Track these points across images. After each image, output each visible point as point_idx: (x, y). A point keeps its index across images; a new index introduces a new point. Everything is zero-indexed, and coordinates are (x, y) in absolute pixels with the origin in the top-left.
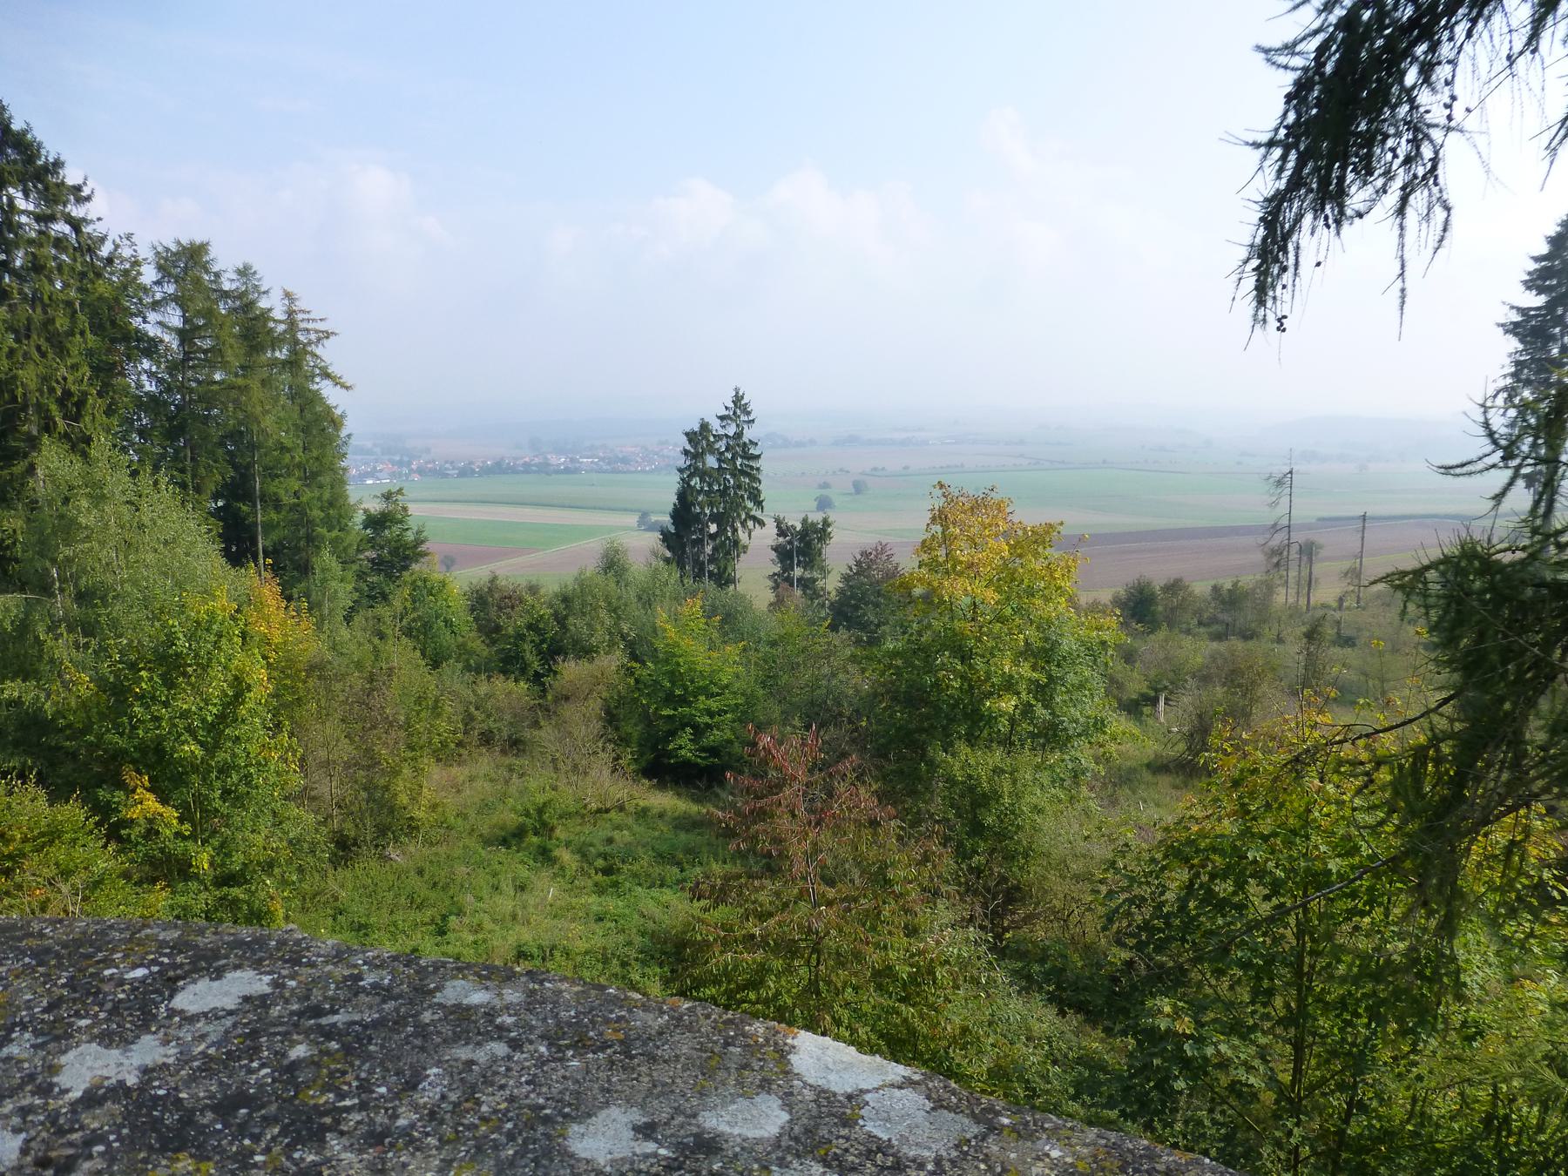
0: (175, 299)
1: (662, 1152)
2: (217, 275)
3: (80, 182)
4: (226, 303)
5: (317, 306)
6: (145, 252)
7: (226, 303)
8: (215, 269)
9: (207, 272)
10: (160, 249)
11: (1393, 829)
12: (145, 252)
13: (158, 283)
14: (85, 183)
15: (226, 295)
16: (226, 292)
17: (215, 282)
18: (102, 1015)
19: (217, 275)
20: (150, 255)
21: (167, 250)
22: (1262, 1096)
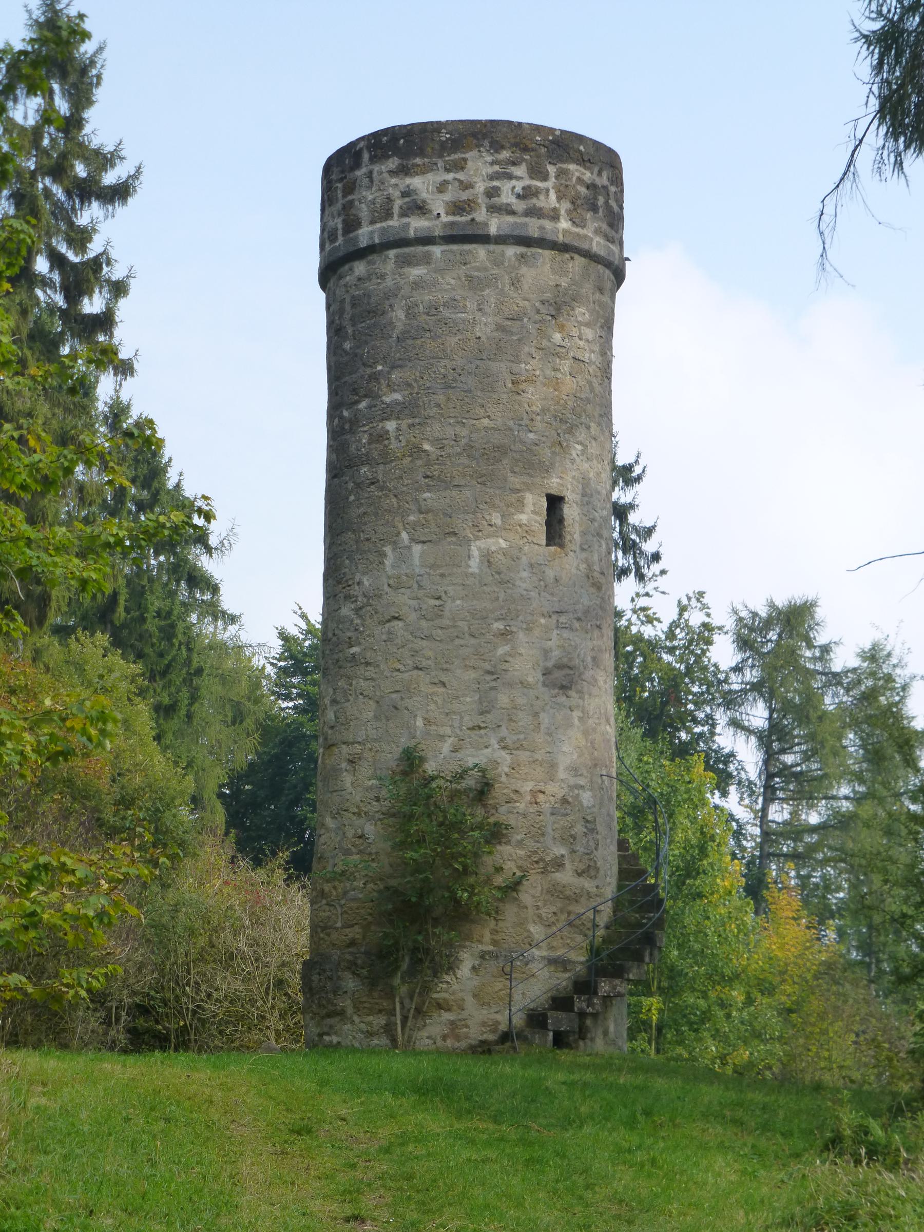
0: (756, 687)
1: (30, 990)
2: (826, 649)
3: (631, 460)
4: (835, 695)
5: (641, 483)
6: (722, 617)
7: (835, 695)
8: (821, 638)
9: (810, 646)
10: (744, 614)
11: (810, 656)
12: (722, 617)
13: (737, 669)
14: (637, 462)
15: (835, 679)
16: (835, 675)
17: (821, 659)
18: (68, 907)
19: (826, 649)
20: (730, 623)
21: (755, 615)
22: (709, 1036)
